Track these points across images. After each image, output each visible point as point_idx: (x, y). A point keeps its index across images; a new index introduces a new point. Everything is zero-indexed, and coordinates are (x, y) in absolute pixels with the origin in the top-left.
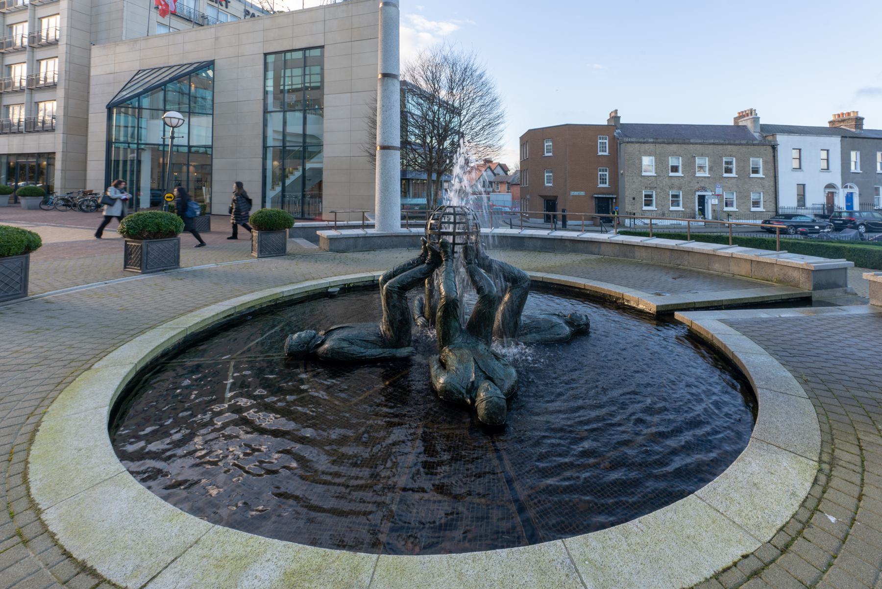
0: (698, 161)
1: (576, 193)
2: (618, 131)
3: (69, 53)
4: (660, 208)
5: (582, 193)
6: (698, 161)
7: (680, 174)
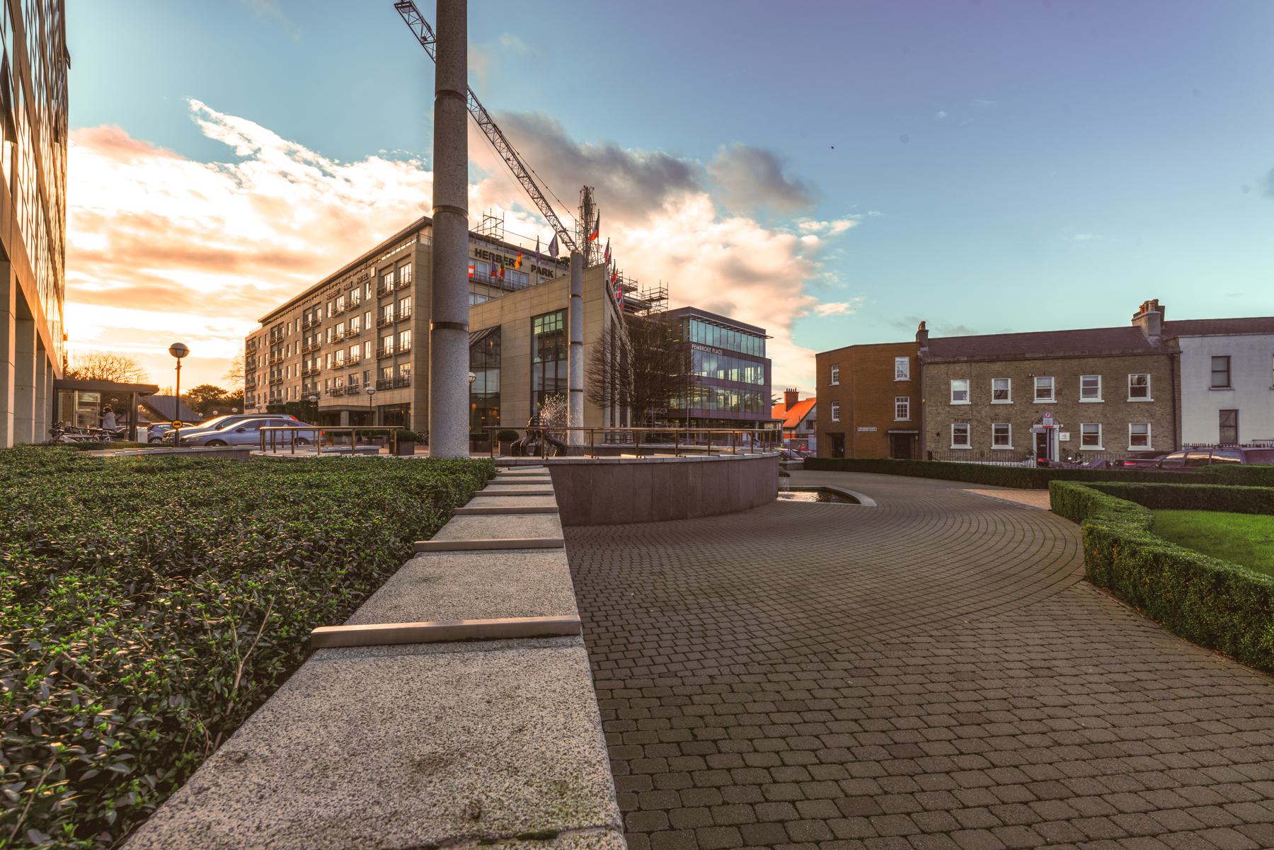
0: (995, 385)
1: (865, 429)
2: (926, 349)
3: (417, 326)
4: (977, 446)
5: (874, 429)
6: (995, 385)
7: (1009, 401)
